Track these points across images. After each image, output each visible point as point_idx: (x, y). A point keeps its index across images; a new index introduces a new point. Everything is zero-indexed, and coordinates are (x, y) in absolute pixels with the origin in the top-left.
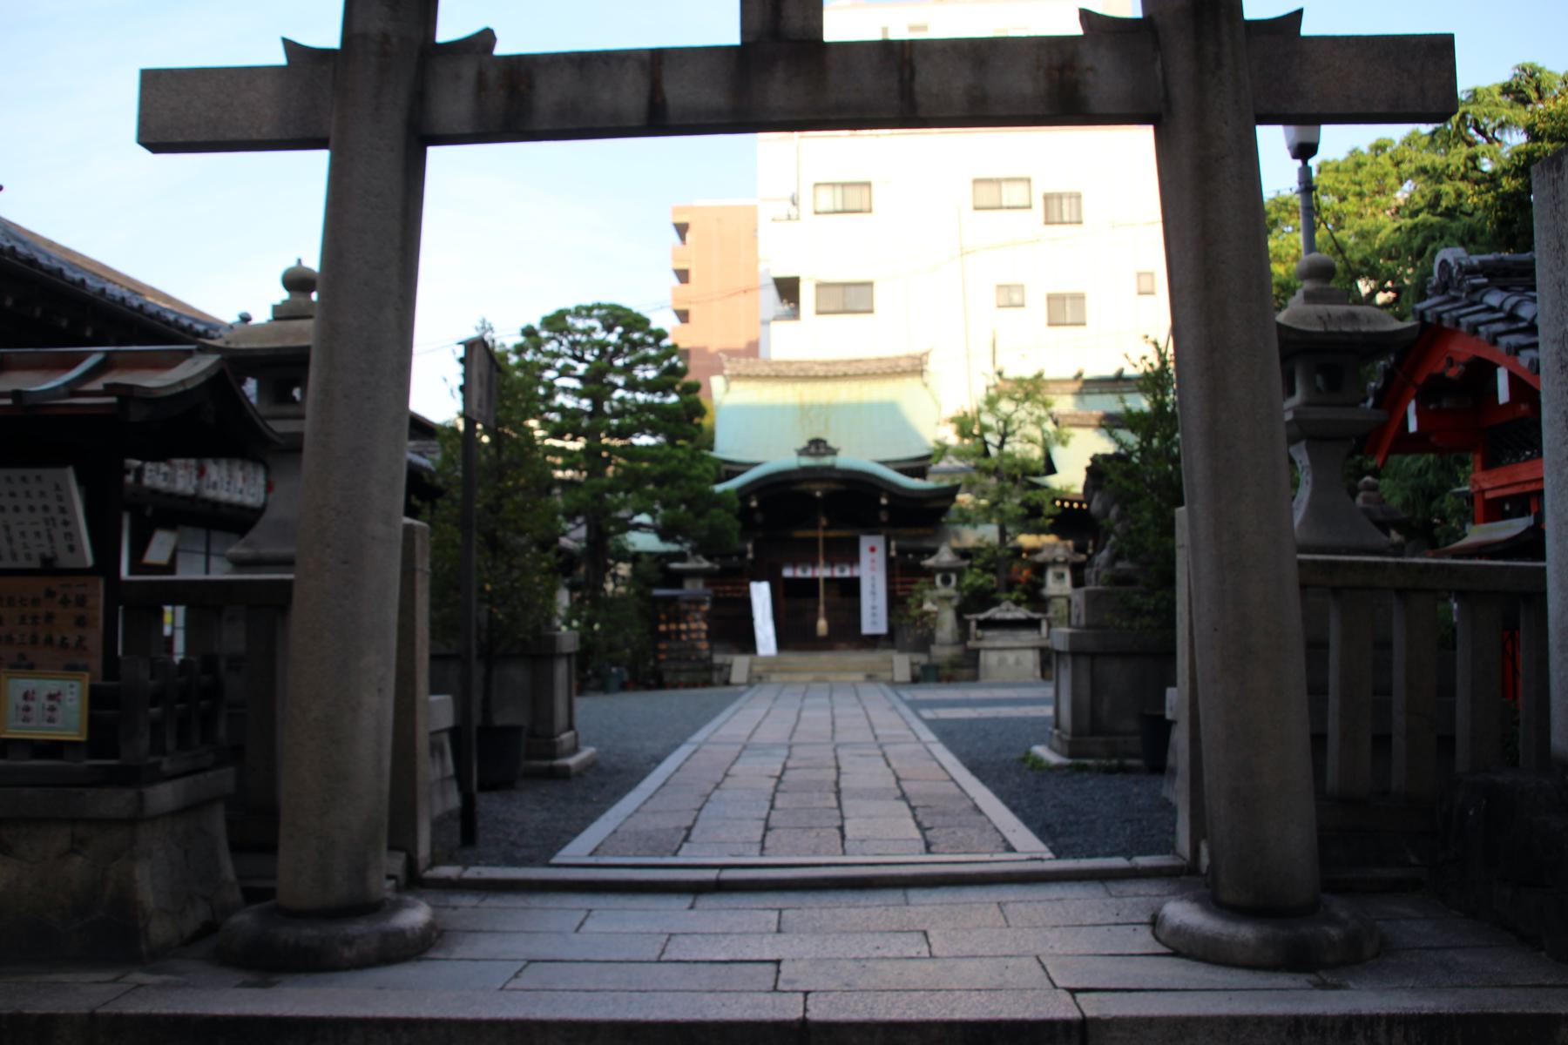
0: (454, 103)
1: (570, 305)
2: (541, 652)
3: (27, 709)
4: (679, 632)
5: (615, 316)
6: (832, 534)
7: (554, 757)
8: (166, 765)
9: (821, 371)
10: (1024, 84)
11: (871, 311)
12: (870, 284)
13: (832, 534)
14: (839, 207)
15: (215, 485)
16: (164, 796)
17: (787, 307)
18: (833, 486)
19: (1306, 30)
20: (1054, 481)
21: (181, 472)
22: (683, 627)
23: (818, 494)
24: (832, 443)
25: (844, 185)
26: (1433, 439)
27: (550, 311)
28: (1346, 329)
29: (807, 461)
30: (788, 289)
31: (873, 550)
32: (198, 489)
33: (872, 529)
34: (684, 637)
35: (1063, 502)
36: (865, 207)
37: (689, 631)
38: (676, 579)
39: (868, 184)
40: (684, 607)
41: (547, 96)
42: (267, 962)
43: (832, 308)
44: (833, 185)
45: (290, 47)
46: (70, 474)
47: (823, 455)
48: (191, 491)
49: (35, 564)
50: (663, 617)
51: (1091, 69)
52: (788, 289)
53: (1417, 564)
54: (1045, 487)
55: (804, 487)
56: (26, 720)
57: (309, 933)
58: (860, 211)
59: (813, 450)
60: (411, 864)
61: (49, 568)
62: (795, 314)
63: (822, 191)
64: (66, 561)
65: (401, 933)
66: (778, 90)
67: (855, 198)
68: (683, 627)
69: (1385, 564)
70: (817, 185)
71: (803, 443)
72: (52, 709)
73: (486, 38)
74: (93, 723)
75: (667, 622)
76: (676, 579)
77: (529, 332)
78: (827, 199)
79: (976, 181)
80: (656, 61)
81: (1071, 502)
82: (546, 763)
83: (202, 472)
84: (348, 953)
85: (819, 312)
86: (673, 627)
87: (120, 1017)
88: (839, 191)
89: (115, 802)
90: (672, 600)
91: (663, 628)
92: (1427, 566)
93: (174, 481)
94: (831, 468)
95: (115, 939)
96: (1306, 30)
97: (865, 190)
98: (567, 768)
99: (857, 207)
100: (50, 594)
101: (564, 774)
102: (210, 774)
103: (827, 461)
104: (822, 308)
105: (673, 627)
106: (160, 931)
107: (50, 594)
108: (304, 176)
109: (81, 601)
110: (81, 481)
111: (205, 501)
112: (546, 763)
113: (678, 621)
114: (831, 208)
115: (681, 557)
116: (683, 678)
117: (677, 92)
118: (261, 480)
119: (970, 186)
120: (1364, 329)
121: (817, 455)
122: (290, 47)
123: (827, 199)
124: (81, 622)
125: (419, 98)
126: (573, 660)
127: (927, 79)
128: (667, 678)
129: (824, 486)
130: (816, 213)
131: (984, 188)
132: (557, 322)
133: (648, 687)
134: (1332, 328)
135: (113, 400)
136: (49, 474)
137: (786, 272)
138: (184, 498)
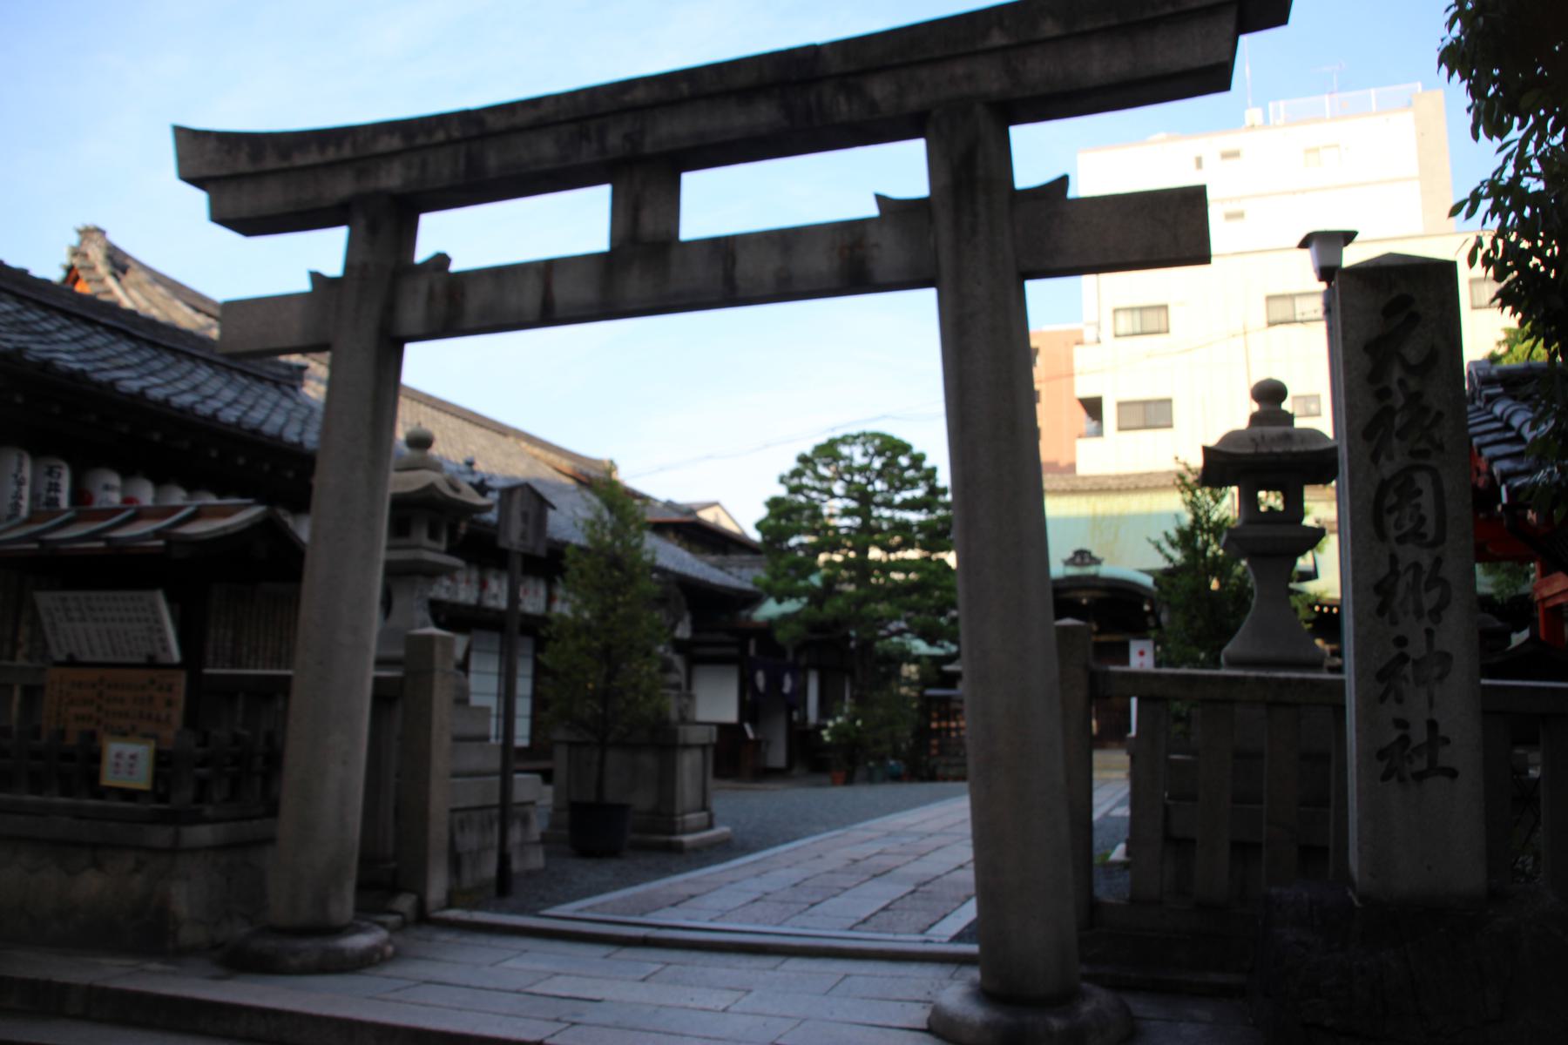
0: (412, 312)
1: (838, 434)
2: (662, 739)
3: (117, 765)
4: (949, 730)
5: (891, 447)
6: (1104, 638)
7: (673, 833)
8: (209, 811)
9: (1113, 484)
10: (820, 262)
11: (1170, 426)
12: (1169, 401)
13: (1104, 638)
14: (1138, 329)
15: (495, 597)
16: (202, 834)
17: (1094, 424)
18: (1098, 594)
19: (1072, 193)
20: (1311, 587)
21: (462, 586)
22: (953, 724)
23: (1084, 601)
24: (1095, 553)
25: (1142, 309)
26: (1490, 550)
27: (822, 439)
28: (1278, 449)
29: (1072, 571)
30: (1093, 407)
31: (1142, 653)
32: (480, 600)
33: (1141, 634)
34: (953, 734)
35: (1321, 607)
36: (1163, 327)
37: (958, 729)
39: (1165, 307)
41: (474, 301)
42: (241, 962)
43: (1134, 424)
44: (1132, 309)
45: (881, 199)
46: (159, 597)
47: (1088, 564)
48: (472, 601)
49: (142, 660)
51: (877, 245)
52: (1093, 407)
53: (1278, 679)
54: (1299, 592)
55: (1071, 595)
56: (131, 773)
57: (270, 944)
58: (1158, 332)
59: (1078, 560)
60: (421, 905)
61: (152, 664)
62: (1099, 433)
63: (1121, 317)
64: (162, 658)
65: (342, 951)
66: (634, 285)
67: (1152, 320)
69: (1244, 678)
70: (1116, 311)
71: (1069, 554)
72: (131, 766)
73: (441, 260)
74: (157, 777)
75: (939, 720)
77: (803, 459)
78: (1126, 323)
79: (1269, 298)
80: (548, 269)
81: (1330, 608)
82: (664, 838)
83: (483, 585)
84: (294, 962)
85: (1120, 429)
86: (944, 724)
87: (105, 990)
88: (1137, 315)
89: (160, 836)
90: (946, 700)
91: (934, 725)
92: (1288, 680)
93: (456, 593)
94: (1095, 577)
95: (152, 936)
96: (1072, 193)
97: (1163, 313)
98: (681, 844)
99: (1156, 328)
100: (153, 682)
101: (678, 849)
102: (256, 822)
103: (1091, 570)
104: (1124, 425)
105: (944, 724)
106: (188, 935)
107: (153, 682)
108: (918, 310)
109: (170, 689)
110: (170, 600)
111: (488, 610)
112: (664, 838)
113: (948, 720)
114: (1130, 330)
117: (563, 292)
118: (542, 591)
119: (1263, 303)
120: (1295, 449)
121: (1082, 564)
122: (881, 199)
123: (1126, 323)
124: (169, 703)
125: (390, 309)
126: (710, 753)
127: (746, 266)
128: (940, 771)
129: (1090, 593)
130: (1116, 336)
131: (1277, 304)
132: (829, 451)
133: (922, 779)
134: (1264, 450)
135: (160, 543)
136: (146, 595)
137: (1089, 393)
138: (467, 607)
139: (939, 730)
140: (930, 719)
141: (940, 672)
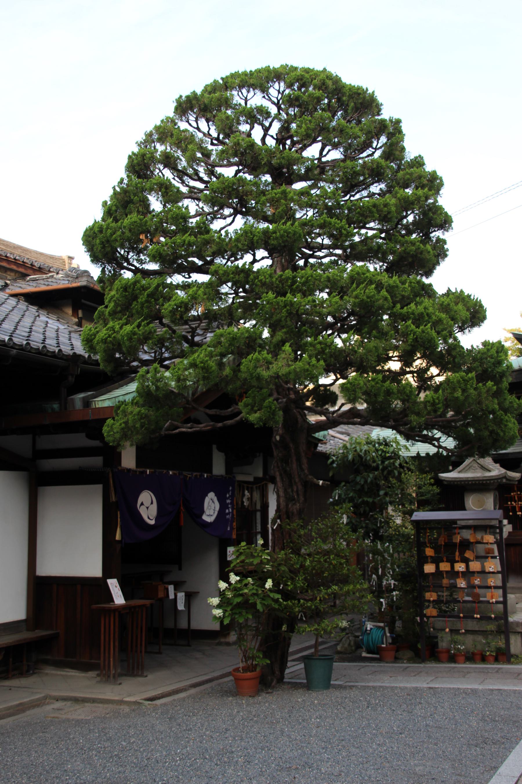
22: (460, 567)
38: (453, 495)
40: (467, 535)
50: (429, 552)
68: (460, 567)
76: (453, 495)
86: (445, 566)
90: (449, 526)
115: (454, 460)
116: (466, 643)
139: (439, 573)
140: (423, 560)
141: (439, 482)
